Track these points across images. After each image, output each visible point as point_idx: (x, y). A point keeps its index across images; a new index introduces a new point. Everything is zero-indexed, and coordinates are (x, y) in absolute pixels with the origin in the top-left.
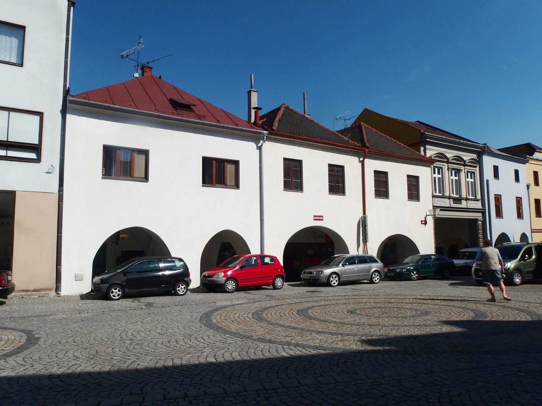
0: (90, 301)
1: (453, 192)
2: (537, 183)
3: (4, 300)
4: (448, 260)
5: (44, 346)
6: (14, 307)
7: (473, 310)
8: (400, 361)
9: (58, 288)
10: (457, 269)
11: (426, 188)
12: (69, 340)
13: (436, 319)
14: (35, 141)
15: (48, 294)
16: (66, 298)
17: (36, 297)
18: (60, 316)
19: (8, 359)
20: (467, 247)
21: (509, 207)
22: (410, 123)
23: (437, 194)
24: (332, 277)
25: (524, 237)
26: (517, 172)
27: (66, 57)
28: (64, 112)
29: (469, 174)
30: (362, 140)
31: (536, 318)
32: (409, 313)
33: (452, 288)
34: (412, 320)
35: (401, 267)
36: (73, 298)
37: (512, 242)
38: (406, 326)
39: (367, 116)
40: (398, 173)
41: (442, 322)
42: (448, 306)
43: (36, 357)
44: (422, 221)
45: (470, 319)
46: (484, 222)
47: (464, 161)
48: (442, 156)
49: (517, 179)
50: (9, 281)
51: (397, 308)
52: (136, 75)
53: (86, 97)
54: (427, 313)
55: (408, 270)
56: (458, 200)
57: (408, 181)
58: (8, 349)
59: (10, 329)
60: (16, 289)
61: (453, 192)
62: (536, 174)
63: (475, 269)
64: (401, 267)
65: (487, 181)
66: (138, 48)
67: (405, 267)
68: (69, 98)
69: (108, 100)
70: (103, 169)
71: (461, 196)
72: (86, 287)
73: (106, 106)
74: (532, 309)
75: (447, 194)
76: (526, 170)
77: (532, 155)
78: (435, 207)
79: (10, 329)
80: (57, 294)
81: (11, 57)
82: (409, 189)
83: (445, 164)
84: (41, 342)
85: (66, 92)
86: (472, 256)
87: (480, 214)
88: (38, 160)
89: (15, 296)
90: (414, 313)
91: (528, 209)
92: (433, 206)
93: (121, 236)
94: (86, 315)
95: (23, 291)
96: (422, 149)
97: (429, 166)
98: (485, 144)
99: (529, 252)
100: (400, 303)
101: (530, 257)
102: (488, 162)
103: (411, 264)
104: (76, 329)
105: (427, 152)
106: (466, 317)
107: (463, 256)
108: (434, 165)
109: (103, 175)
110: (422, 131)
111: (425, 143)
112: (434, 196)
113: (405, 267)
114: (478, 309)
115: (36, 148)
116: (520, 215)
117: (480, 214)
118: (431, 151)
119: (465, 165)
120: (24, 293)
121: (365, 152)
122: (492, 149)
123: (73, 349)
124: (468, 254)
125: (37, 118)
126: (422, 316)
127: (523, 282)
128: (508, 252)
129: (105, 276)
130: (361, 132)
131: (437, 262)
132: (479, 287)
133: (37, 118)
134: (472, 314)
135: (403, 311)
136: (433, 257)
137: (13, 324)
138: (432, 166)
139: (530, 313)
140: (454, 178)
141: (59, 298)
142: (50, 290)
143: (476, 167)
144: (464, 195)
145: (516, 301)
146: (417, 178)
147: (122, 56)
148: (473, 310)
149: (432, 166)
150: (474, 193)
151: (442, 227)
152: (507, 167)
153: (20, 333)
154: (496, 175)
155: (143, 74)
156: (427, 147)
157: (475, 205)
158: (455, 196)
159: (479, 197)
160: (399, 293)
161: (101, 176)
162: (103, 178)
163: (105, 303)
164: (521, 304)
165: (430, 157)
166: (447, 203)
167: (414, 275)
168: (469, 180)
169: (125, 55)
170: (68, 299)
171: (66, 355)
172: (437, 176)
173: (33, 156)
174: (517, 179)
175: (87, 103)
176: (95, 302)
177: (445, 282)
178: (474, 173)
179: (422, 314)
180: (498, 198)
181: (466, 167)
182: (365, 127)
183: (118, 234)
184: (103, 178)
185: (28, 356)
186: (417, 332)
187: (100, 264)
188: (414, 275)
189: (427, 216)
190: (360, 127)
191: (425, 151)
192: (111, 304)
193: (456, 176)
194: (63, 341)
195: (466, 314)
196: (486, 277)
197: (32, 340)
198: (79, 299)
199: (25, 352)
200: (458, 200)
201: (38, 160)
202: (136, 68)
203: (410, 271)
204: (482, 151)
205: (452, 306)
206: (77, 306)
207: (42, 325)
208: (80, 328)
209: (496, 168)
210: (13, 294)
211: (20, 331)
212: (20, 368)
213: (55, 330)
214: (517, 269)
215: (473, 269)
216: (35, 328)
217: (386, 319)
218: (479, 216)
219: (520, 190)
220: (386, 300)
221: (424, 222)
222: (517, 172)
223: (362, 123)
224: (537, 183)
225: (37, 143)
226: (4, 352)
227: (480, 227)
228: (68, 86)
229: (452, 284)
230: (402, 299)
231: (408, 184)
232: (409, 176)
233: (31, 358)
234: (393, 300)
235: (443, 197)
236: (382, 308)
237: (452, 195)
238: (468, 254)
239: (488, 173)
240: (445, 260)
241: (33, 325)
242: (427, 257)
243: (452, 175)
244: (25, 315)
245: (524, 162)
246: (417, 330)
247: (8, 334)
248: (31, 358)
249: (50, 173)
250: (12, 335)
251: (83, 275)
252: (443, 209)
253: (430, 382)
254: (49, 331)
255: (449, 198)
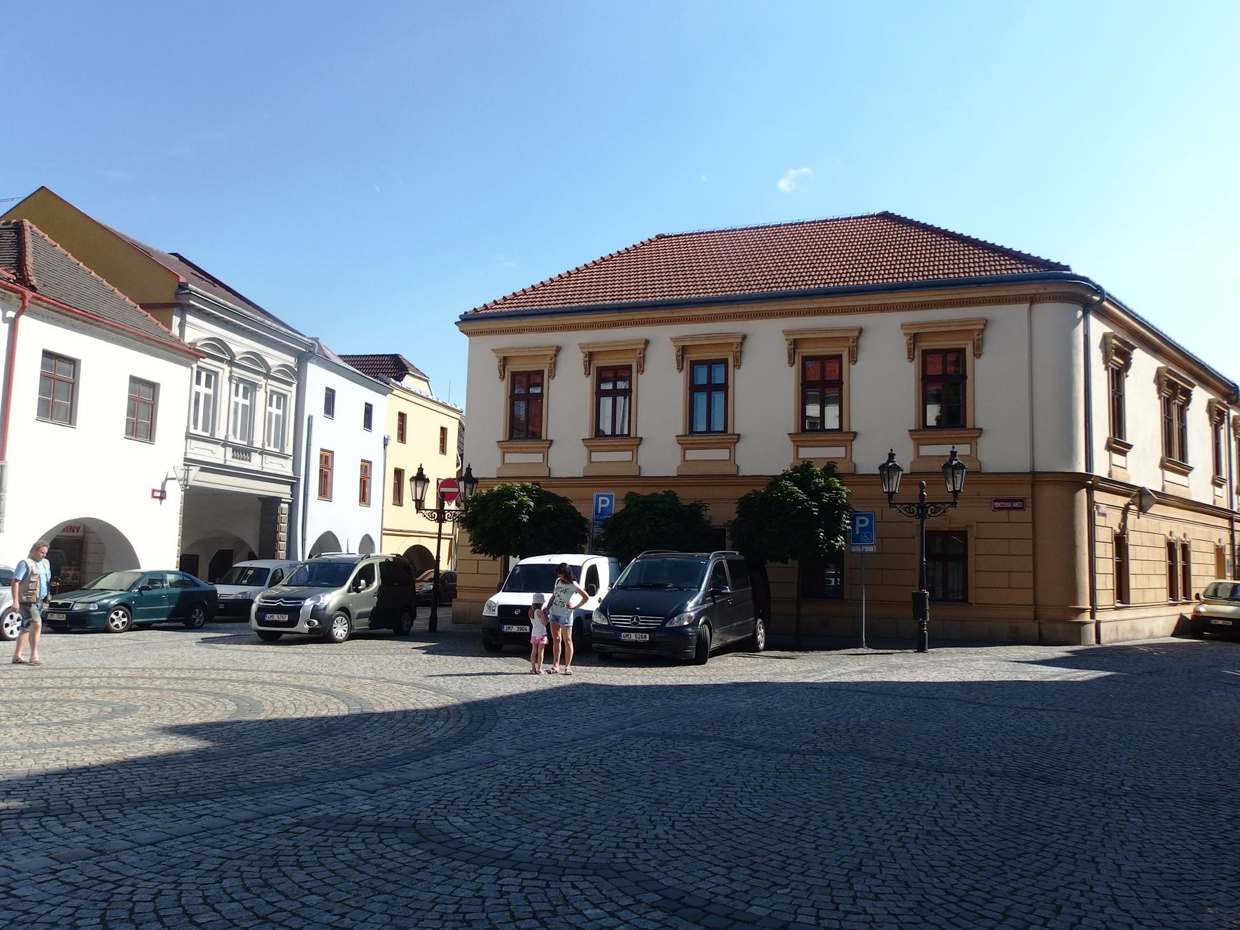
1: (235, 433)
2: (402, 437)
4: (204, 585)
7: (236, 699)
8: (25, 834)
10: (222, 606)
11: (173, 412)
13: (145, 722)
20: (252, 557)
21: (345, 479)
22: (157, 253)
23: (199, 432)
24: (11, 617)
25: (367, 543)
26: (368, 409)
29: (275, 397)
30: (19, 264)
31: (356, 709)
32: (82, 712)
33: (203, 649)
34: (85, 730)
35: (86, 599)
37: (344, 550)
38: (67, 744)
39: (44, 204)
40: (107, 367)
41: (164, 729)
42: (182, 691)
44: (154, 491)
45: (224, 718)
46: (292, 506)
47: (268, 368)
48: (219, 346)
49: (368, 424)
51: (54, 700)
54: (127, 710)
55: (101, 608)
56: (243, 452)
57: (42, 391)
61: (235, 433)
62: (402, 417)
63: (260, 609)
64: (86, 599)
65: (310, 418)
67: (97, 598)
71: (251, 442)
74: (356, 691)
75: (220, 434)
76: (387, 406)
77: (400, 378)
78: (189, 462)
82: (132, 411)
83: (225, 366)
86: (258, 578)
87: (287, 488)
90: (95, 711)
91: (381, 486)
92: (186, 459)
96: (176, 320)
97: (188, 365)
98: (316, 340)
99: (367, 573)
100: (65, 687)
101: (369, 582)
102: (318, 378)
103: (114, 593)
105: (188, 330)
106: (216, 713)
107: (244, 577)
108: (200, 364)
110: (182, 279)
111: (184, 309)
112: (189, 436)
113: (97, 598)
114: (247, 695)
116: (364, 498)
117: (287, 488)
118: (197, 331)
119: (267, 376)
121: (23, 298)
122: (328, 353)
124: (251, 572)
126: (113, 717)
127: (351, 636)
128: (328, 572)
130: (20, 244)
131: (178, 590)
132: (261, 647)
134: (232, 707)
135: (67, 708)
136: (170, 578)
138: (194, 366)
139: (346, 698)
140: (240, 400)
143: (290, 384)
144: (258, 443)
145: (329, 675)
146: (154, 387)
149: (194, 366)
150: (281, 442)
151: (200, 508)
152: (352, 395)
154: (329, 408)
156: (189, 318)
157: (279, 467)
158: (238, 441)
159: (289, 450)
160: (70, 663)
164: (337, 681)
165: (193, 344)
166: (217, 455)
167: (119, 620)
168: (274, 410)
172: (203, 389)
174: (368, 424)
177: (191, 635)
178: (285, 396)
179: (115, 713)
180: (327, 459)
181: (270, 382)
182: (33, 234)
186: (90, 758)
188: (119, 620)
189: (167, 479)
190: (19, 229)
191: (182, 326)
193: (245, 397)
195: (219, 706)
196: (279, 627)
200: (243, 452)
203: (107, 609)
204: (307, 353)
205: (190, 691)
209: (330, 395)
214: (343, 610)
215: (254, 607)
217: (15, 732)
218: (283, 491)
219: (368, 444)
220: (29, 681)
221: (158, 494)
222: (368, 409)
223: (27, 223)
224: (402, 437)
227: (285, 517)
229: (205, 641)
230: (73, 678)
231: (130, 399)
232: (134, 380)
234: (49, 682)
235: (212, 440)
236: (12, 702)
237: (231, 439)
238: (251, 572)
239: (314, 404)
240: (197, 585)
242: (155, 578)
243: (237, 394)
245: (385, 391)
246: (91, 752)
252: (208, 467)
253: (90, 878)
255: (225, 444)
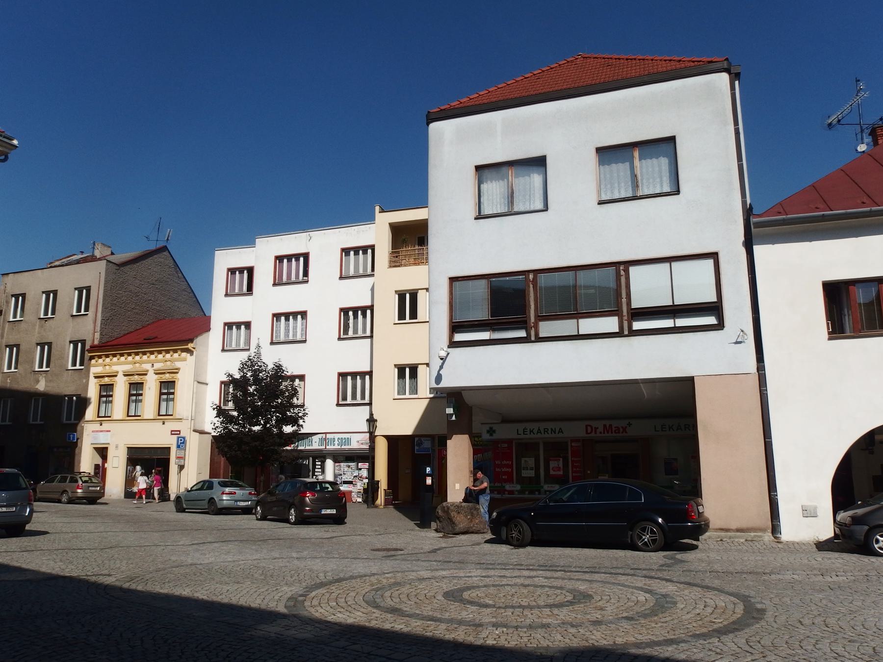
0: (837, 555)
3: (695, 542)
5: (775, 626)
6: (713, 555)
7: (570, 591)
9: (775, 529)
12: (816, 622)
14: (710, 297)
15: (760, 537)
16: (792, 546)
17: (742, 540)
18: (788, 576)
19: (724, 638)
27: (740, 159)
28: (748, 245)
36: (804, 547)
43: (766, 641)
50: (700, 514)
52: (862, 148)
53: (782, 210)
58: (720, 622)
59: (714, 589)
60: (711, 526)
66: (858, 100)
68: (753, 220)
69: (821, 206)
70: (828, 324)
72: (825, 529)
73: (866, 212)
79: (714, 589)
80: (775, 538)
81: (662, 186)
84: (769, 615)
85: (748, 212)
88: (720, 326)
89: (710, 538)
93: (878, 437)
94: (835, 578)
95: (722, 530)
104: (824, 602)
109: (829, 333)
115: (715, 308)
120: (723, 534)
123: (829, 638)
125: (710, 262)
129: (860, 511)
133: (710, 262)
137: (716, 581)
141: (780, 546)
142: (763, 530)
147: (830, 124)
148: (570, 591)
153: (732, 598)
155: (875, 143)
161: (826, 336)
162: (830, 339)
163: (866, 559)
169: (835, 122)
170: (794, 548)
171: (817, 646)
173: (711, 320)
175: (784, 220)
176: (845, 556)
183: (871, 434)
184: (830, 339)
185: (753, 639)
187: (844, 487)
192: (877, 563)
194: (806, 621)
197: (753, 614)
198: (815, 549)
199: (747, 630)
201: (720, 326)
202: (859, 136)
206: (814, 562)
207: (762, 588)
208: (830, 601)
210: (707, 534)
211: (731, 594)
212: (745, 657)
213: (787, 600)
216: (752, 593)
225: (715, 300)
226: (715, 626)
228: (748, 202)
233: (759, 642)
241: (748, 587)
244: (731, 569)
247: (713, 597)
248: (759, 642)
249: (740, 342)
250: (722, 601)
251: (816, 508)
254: (776, 600)
